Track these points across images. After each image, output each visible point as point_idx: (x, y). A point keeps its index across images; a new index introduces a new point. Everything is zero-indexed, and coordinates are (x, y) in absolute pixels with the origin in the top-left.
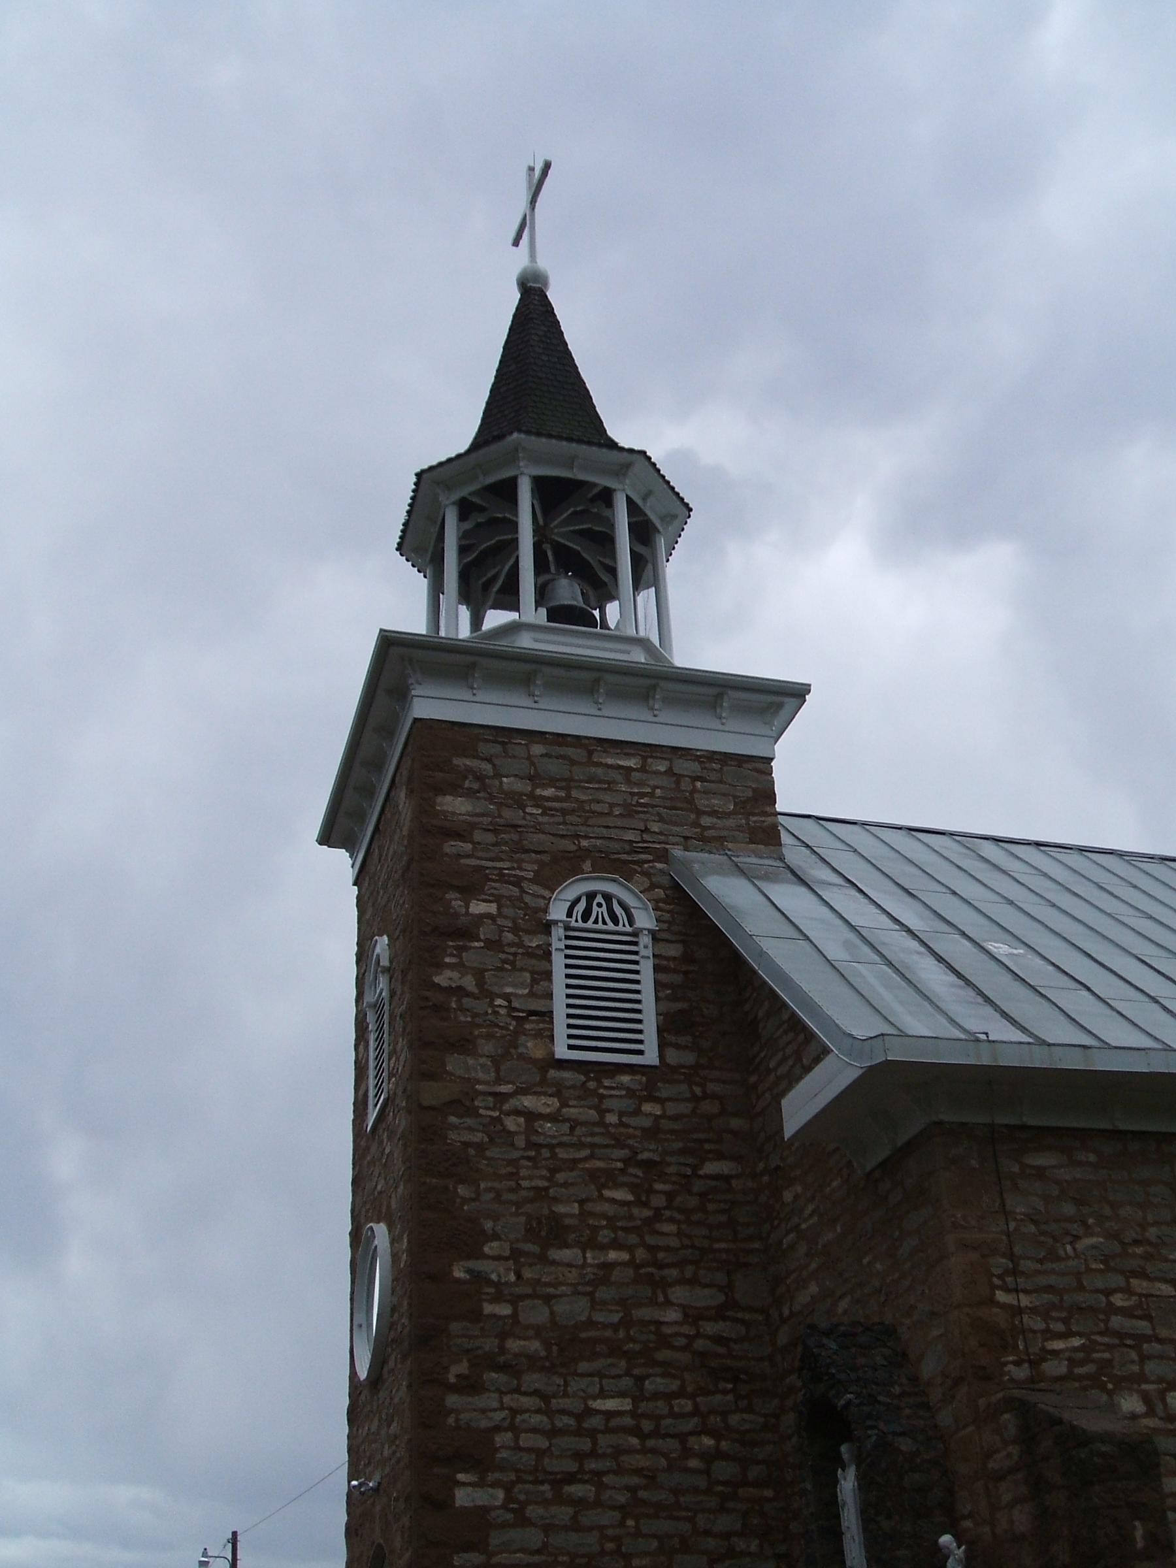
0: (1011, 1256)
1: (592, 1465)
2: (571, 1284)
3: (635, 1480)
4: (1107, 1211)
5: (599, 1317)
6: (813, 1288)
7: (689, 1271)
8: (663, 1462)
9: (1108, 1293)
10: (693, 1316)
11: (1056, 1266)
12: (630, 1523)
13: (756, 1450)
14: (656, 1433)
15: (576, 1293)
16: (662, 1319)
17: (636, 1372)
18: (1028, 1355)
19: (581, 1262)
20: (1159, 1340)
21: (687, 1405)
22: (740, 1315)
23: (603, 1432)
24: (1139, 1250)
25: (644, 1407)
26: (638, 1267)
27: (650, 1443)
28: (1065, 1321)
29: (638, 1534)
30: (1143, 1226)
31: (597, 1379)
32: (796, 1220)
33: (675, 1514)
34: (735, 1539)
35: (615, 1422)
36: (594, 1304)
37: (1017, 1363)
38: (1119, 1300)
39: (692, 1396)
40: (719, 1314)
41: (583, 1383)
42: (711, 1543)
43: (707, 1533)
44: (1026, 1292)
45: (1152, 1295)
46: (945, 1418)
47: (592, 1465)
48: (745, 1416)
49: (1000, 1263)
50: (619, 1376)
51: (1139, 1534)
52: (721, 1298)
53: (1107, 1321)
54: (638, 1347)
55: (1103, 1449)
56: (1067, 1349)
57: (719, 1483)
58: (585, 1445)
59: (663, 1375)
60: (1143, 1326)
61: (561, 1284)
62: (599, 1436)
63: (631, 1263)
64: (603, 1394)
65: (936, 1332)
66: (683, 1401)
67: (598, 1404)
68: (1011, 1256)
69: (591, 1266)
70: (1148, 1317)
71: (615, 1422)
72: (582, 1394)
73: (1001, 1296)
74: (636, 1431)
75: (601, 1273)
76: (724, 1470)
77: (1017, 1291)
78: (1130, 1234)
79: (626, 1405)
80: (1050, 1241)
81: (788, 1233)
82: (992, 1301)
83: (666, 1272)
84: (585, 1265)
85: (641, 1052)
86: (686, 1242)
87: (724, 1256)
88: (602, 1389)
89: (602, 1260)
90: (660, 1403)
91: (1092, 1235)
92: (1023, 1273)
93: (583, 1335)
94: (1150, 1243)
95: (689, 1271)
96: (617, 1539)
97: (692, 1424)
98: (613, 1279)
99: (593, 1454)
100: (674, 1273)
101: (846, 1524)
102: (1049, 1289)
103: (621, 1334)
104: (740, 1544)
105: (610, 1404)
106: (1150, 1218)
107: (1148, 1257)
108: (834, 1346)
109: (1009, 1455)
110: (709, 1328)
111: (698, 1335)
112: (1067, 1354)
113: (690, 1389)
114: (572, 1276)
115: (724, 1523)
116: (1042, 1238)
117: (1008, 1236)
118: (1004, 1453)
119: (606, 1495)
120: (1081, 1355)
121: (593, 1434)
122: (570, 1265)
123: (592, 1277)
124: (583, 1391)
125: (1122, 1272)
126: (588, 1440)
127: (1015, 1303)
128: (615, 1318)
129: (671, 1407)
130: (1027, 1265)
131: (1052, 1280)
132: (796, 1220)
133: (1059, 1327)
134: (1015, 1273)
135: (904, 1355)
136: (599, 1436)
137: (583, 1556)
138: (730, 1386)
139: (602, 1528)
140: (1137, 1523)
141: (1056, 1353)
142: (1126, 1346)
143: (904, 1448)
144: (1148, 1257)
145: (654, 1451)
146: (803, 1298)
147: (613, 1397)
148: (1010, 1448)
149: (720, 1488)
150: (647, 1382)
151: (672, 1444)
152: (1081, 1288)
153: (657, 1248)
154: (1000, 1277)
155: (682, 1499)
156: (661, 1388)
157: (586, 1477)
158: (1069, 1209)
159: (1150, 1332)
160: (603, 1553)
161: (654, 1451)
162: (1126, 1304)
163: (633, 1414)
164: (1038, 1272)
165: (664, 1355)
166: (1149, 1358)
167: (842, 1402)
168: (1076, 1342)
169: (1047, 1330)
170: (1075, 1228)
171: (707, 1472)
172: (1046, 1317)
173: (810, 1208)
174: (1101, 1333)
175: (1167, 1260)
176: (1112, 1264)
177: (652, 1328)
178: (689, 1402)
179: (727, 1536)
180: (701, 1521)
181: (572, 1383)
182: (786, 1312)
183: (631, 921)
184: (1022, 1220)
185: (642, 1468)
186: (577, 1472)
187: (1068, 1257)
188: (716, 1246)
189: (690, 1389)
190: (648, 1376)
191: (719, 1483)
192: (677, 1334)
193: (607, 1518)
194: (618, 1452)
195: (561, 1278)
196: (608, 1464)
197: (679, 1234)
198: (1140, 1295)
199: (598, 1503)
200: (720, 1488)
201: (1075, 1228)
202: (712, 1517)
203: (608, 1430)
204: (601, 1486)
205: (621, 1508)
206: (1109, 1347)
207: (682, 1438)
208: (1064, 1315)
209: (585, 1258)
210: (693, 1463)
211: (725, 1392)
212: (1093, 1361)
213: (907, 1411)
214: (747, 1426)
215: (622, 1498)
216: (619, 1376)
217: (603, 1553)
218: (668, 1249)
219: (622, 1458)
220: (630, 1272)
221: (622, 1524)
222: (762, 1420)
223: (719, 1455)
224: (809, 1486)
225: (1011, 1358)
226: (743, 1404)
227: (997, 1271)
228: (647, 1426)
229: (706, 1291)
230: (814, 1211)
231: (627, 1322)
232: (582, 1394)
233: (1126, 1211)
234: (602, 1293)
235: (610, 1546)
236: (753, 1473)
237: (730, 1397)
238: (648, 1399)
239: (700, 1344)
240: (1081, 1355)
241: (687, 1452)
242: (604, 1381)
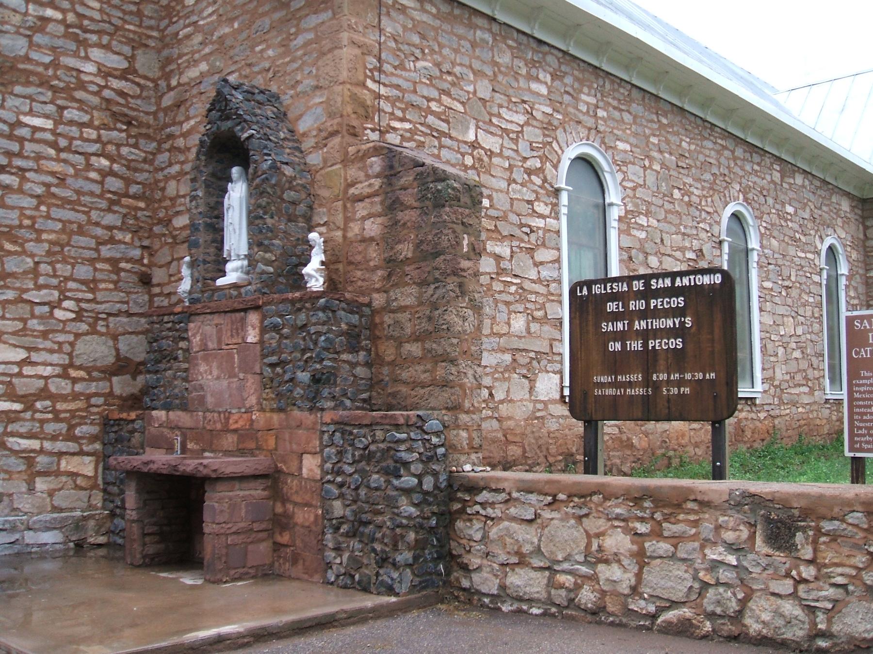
0: (379, 60)
1: (18, 162)
2: (14, 26)
3: (49, 179)
4: (436, 48)
5: (34, 56)
6: (204, 67)
7: (105, 39)
8: (71, 171)
9: (429, 100)
10: (105, 72)
11: (403, 73)
12: (43, 208)
13: (137, 174)
14: (68, 149)
15: (17, 33)
16: (82, 69)
17: (59, 102)
18: (380, 126)
19: (24, 11)
20: (451, 138)
21: (92, 134)
22: (137, 80)
23: (30, 141)
24: (449, 78)
25: (61, 129)
26: (68, 26)
27: (63, 155)
28: (403, 111)
29: (48, 217)
30: (454, 64)
31: (28, 101)
32: (194, 18)
33: (76, 207)
34: (115, 231)
35: (38, 135)
36: (31, 45)
37: (373, 130)
38: (434, 106)
39: (98, 128)
40: (123, 75)
41: (18, 102)
42: (99, 231)
43: (97, 224)
44: (385, 85)
45: (452, 109)
46: (314, 159)
47: (18, 162)
48: (133, 150)
49: (372, 62)
50: (45, 103)
51: (465, 242)
52: (125, 65)
53: (426, 117)
54: (62, 85)
55: (455, 185)
56: (402, 129)
57: (110, 192)
58: (15, 147)
59: (78, 109)
60: (443, 127)
61: (6, 23)
62: (26, 143)
63: (63, 22)
64: (31, 113)
65: (318, 100)
66: (90, 131)
67: (26, 119)
68: (379, 60)
69: (32, 16)
70: (447, 122)
71: (38, 135)
72: (15, 110)
73: (369, 83)
74: (54, 145)
75: (39, 23)
76: (112, 183)
77: (379, 82)
78: (446, 67)
79: (49, 124)
80: (403, 56)
81: (185, 27)
82: (364, 85)
83: (88, 36)
84: (26, 14)
86: (105, 18)
87: (131, 36)
88: (31, 110)
89: (41, 13)
90: (74, 128)
91: (426, 60)
92: (384, 72)
93: (21, 66)
94: (456, 76)
95: (105, 39)
96: (32, 218)
97: (95, 148)
98: (48, 30)
99: (20, 155)
100: (94, 38)
101: (230, 221)
102: (398, 87)
103: (50, 72)
104: (119, 235)
105: (37, 122)
106: (458, 61)
107: (453, 84)
108: (240, 97)
109: (370, 185)
110: (116, 84)
111: (106, 87)
112: (401, 132)
113: (96, 123)
114: (17, 19)
115: (110, 219)
116: (398, 53)
117: (380, 44)
118: (367, 183)
119: (27, 186)
120: (408, 135)
121: (21, 140)
122: (15, 11)
123: (32, 24)
124: (17, 107)
125: (438, 89)
126: (17, 144)
127: (377, 90)
128: (47, 59)
129: (82, 133)
130: (387, 67)
131: (400, 82)
132: (194, 18)
133: (399, 113)
134: (380, 70)
135: (285, 114)
136: (26, 143)
137: (6, 226)
138: (125, 127)
139: (22, 209)
140: (465, 236)
141: (395, 129)
142: (433, 136)
143: (287, 173)
144: (453, 84)
145: (65, 161)
146: (193, 73)
147: (39, 117)
148: (372, 181)
149: (109, 196)
150: (65, 112)
151: (79, 159)
152: (415, 91)
153: (84, 16)
154: (370, 70)
155: (82, 198)
156: (76, 118)
157: (14, 171)
158: (416, 39)
159: (447, 131)
160: (21, 226)
161: (65, 161)
162: (438, 110)
163: (53, 132)
164: (392, 74)
165: (80, 94)
166: (444, 147)
167: (246, 135)
168: (407, 126)
169: (392, 114)
170: (418, 53)
171: (102, 183)
172: (393, 105)
173: (210, 10)
174: (421, 124)
175: (462, 89)
176: (434, 82)
177: (74, 74)
178: (95, 132)
179: (110, 228)
180: (94, 215)
181: (9, 100)
182: (174, 83)
184: (389, 37)
185: (56, 172)
186: (6, 166)
187: (410, 70)
188: (127, 27)
189: (96, 123)
190: (66, 108)
191: (110, 192)
192: (92, 82)
193: (27, 202)
194: (38, 157)
195: (7, 19)
196: (31, 164)
197: (101, 11)
198: (446, 106)
199: (20, 191)
200: (109, 196)
201: (418, 53)
202: (102, 214)
203: (32, 140)
204: (23, 179)
205: (38, 197)
206: (425, 134)
207: (87, 155)
208: (403, 106)
209: (27, 9)
210: (93, 175)
211: (121, 131)
212: (415, 140)
213: (288, 151)
214: (133, 157)
215: (39, 190)
216: (45, 103)
217: (21, 226)
218: (92, 19)
219: (42, 162)
220: (62, 29)
221: (37, 208)
222: (143, 155)
223: (112, 173)
224: (200, 193)
225: (369, 126)
226: (132, 141)
227: (370, 66)
228: (63, 143)
229: (116, 57)
230: (213, 12)
231: (55, 64)
232: (15, 110)
233: (446, 51)
234: (38, 38)
235: (27, 222)
236: (134, 189)
237: (124, 135)
238: (65, 124)
239: (107, 93)
240: (408, 135)
241: (89, 166)
242: (34, 104)
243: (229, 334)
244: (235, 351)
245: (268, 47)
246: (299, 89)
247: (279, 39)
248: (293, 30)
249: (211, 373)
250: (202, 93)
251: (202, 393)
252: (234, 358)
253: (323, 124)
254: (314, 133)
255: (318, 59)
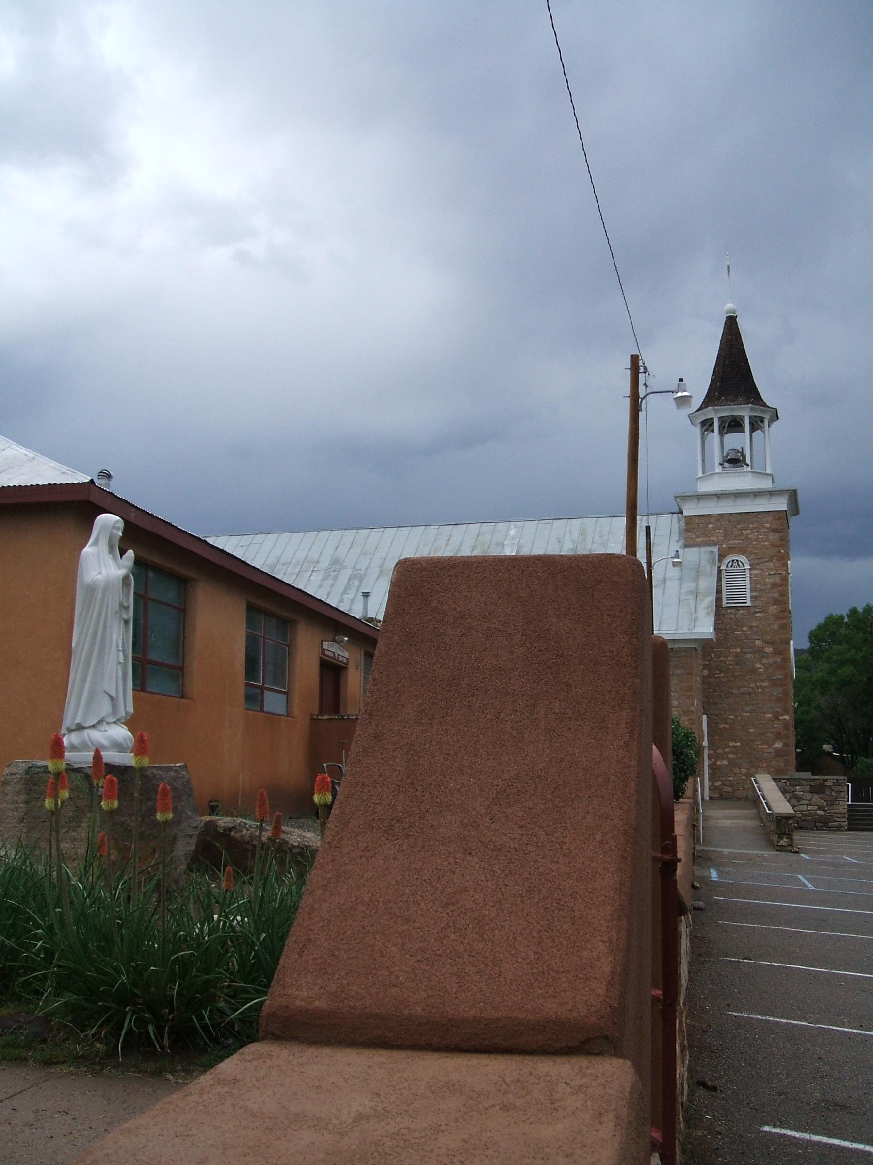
85: (746, 603)
183: (744, 567)
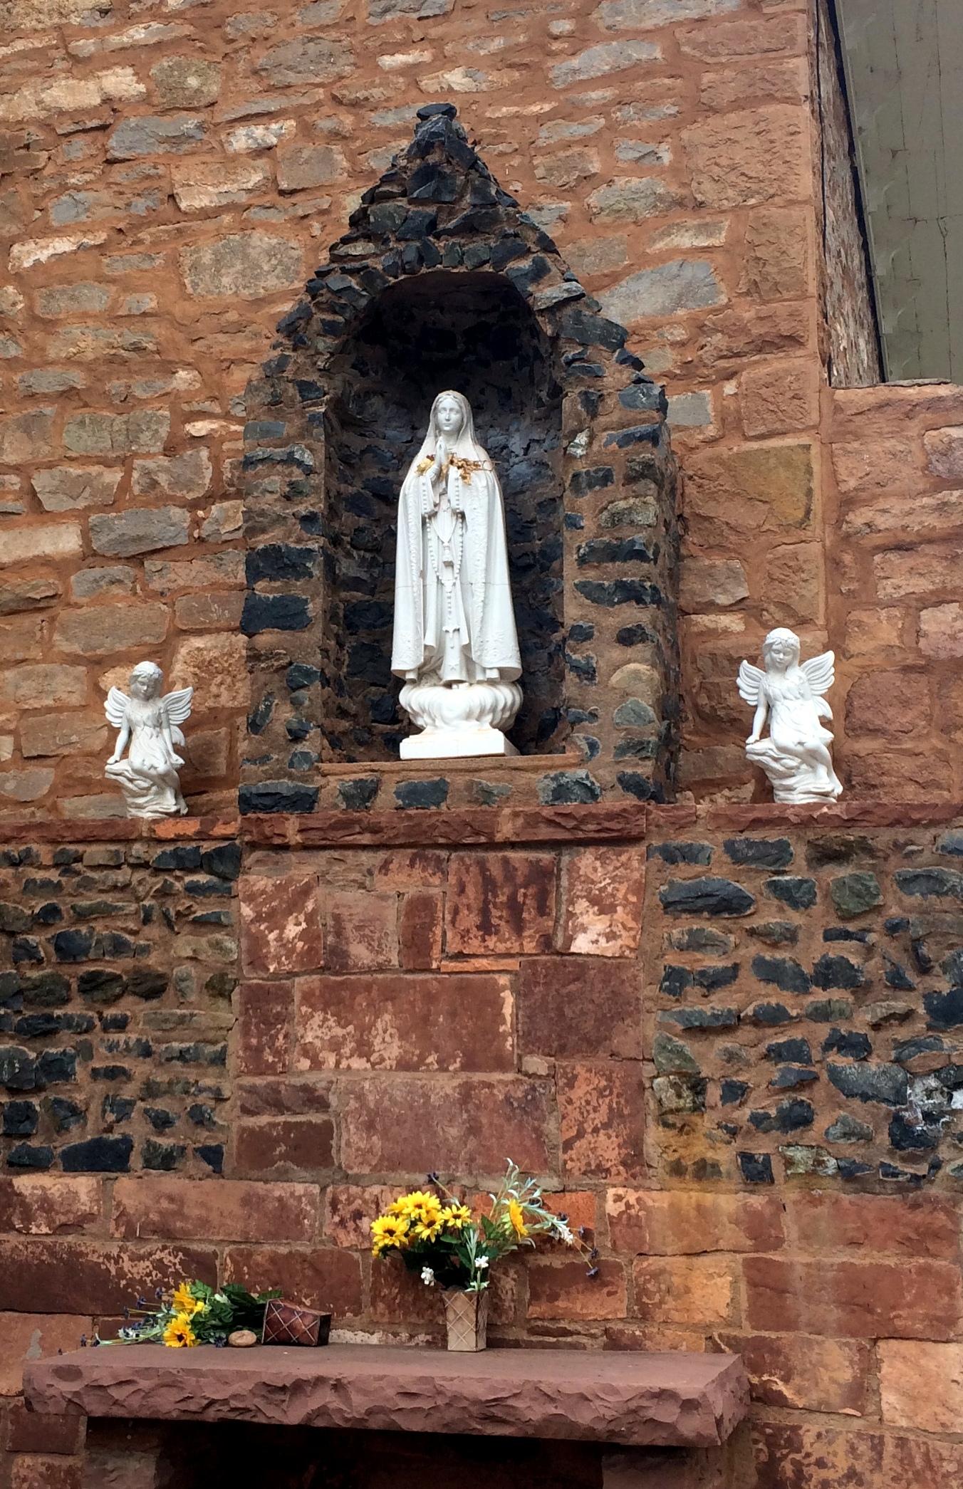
6: (121, 82)
243: (470, 920)
244: (503, 980)
245: (444, 61)
246: (594, 200)
247: (497, 44)
248: (563, 26)
249: (364, 1049)
250: (110, 162)
251: (316, 1118)
252: (498, 1004)
253: (716, 311)
254: (680, 334)
255: (679, 121)
